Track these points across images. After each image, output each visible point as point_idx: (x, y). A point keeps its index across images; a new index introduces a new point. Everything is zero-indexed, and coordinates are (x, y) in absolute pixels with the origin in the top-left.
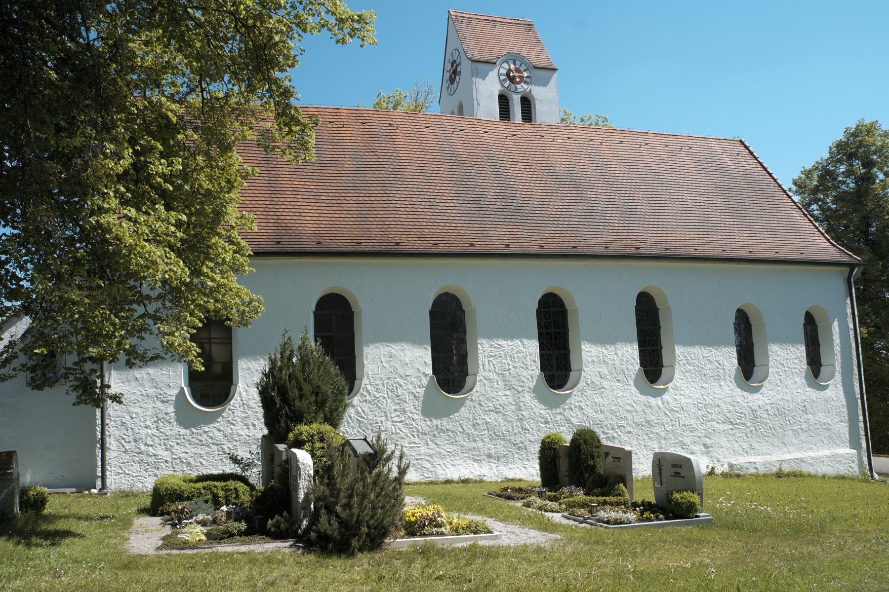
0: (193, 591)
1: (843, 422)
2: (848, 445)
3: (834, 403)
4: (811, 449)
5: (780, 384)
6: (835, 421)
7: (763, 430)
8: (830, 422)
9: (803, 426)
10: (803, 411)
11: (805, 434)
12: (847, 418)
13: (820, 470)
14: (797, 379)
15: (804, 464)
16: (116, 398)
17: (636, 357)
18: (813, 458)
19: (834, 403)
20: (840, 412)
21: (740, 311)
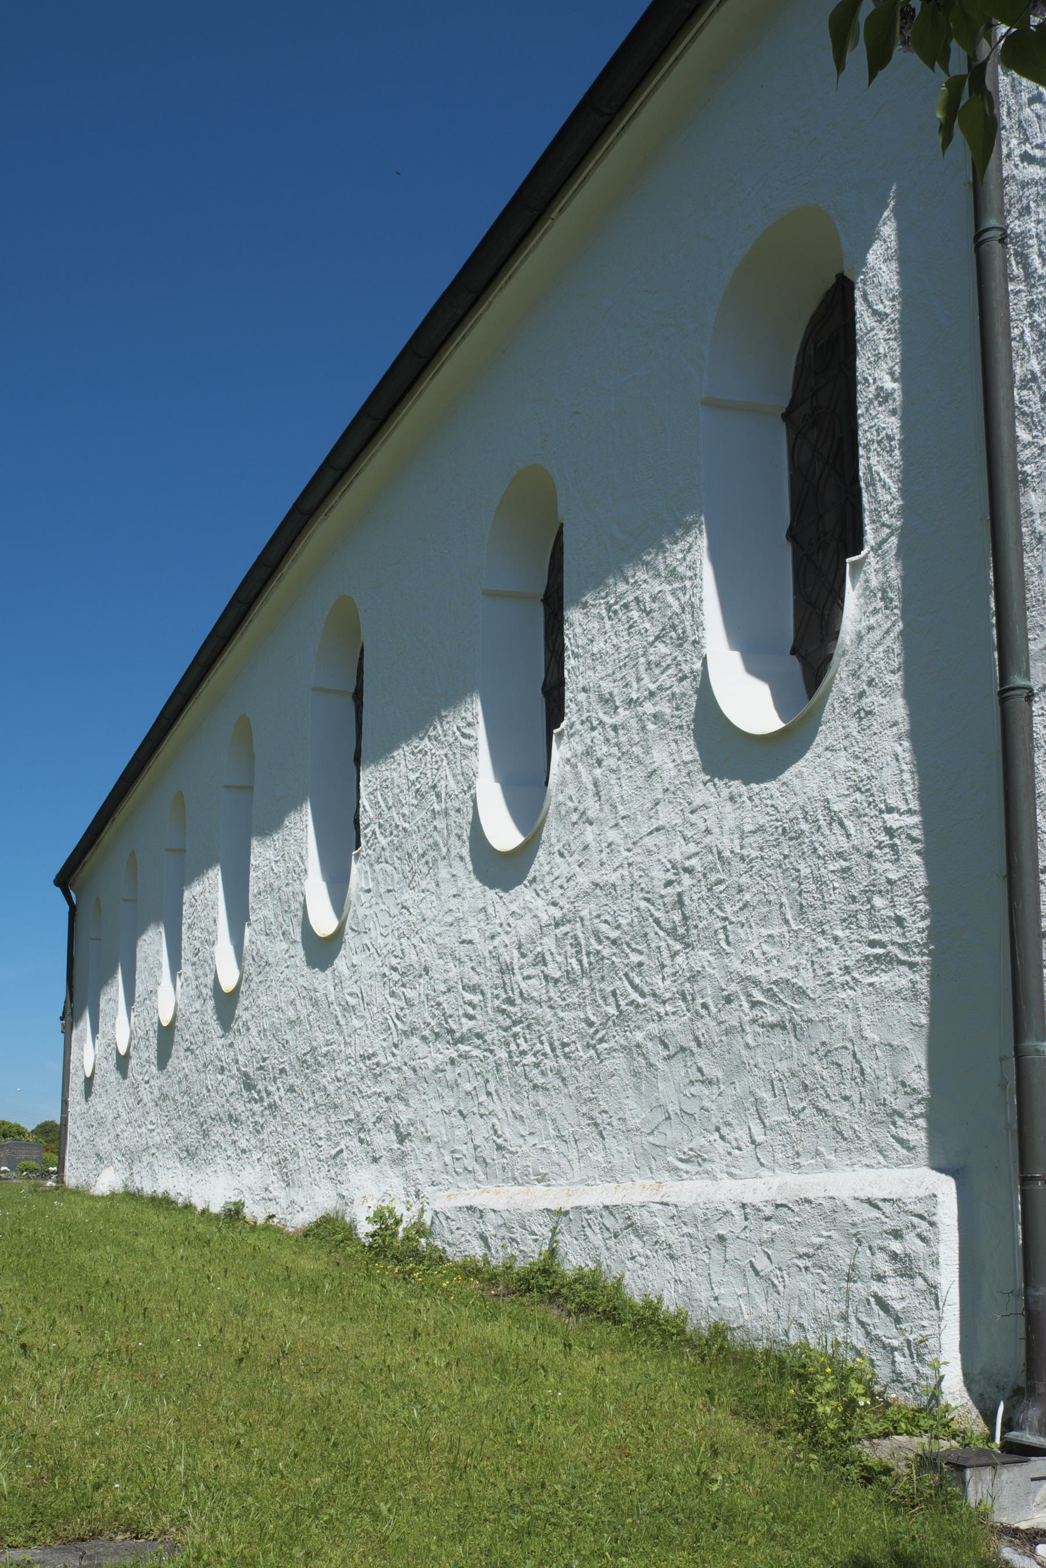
0: (99, 1565)
1: (890, 960)
2: (917, 1136)
3: (836, 841)
4: (696, 1158)
5: (593, 808)
6: (835, 960)
7: (529, 1059)
8: (806, 980)
9: (672, 1024)
10: (672, 932)
11: (678, 1069)
12: (918, 927)
13: (703, 1295)
14: (659, 756)
15: (637, 1245)
16: (945, 1363)
17: (573, 706)
18: (677, 1216)
19: (836, 841)
20: (869, 892)
21: (313, 690)
